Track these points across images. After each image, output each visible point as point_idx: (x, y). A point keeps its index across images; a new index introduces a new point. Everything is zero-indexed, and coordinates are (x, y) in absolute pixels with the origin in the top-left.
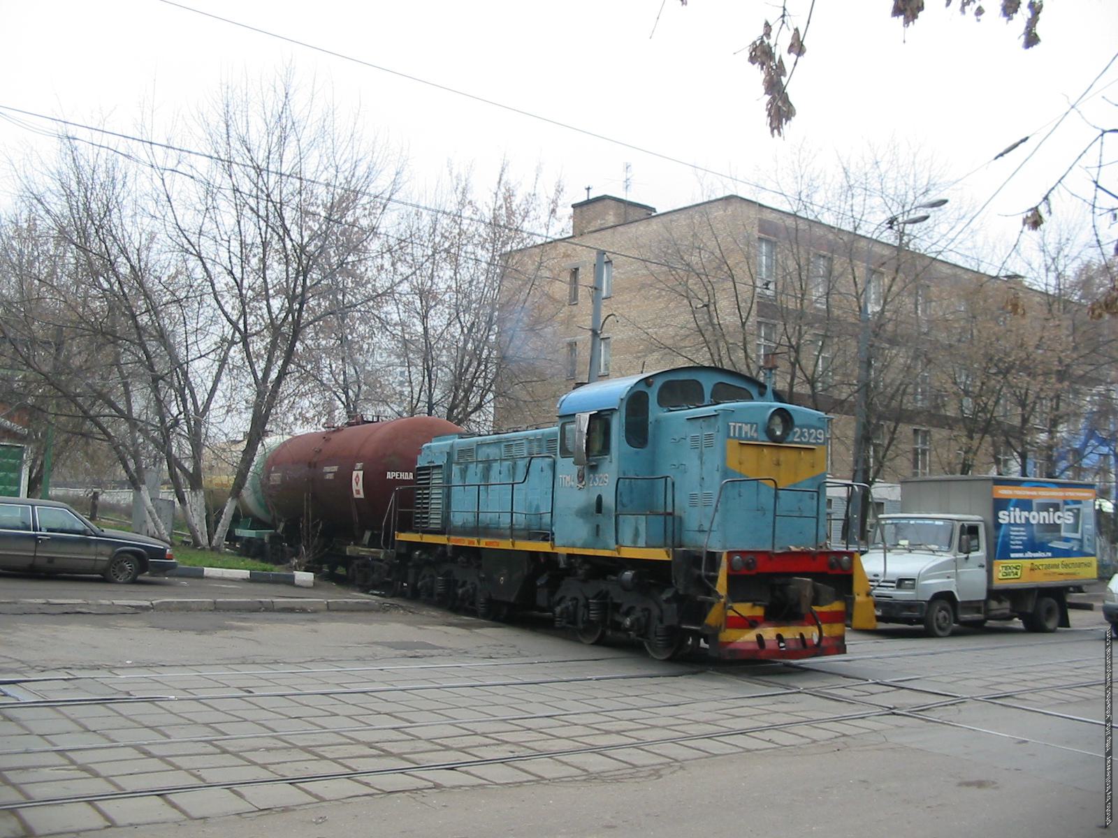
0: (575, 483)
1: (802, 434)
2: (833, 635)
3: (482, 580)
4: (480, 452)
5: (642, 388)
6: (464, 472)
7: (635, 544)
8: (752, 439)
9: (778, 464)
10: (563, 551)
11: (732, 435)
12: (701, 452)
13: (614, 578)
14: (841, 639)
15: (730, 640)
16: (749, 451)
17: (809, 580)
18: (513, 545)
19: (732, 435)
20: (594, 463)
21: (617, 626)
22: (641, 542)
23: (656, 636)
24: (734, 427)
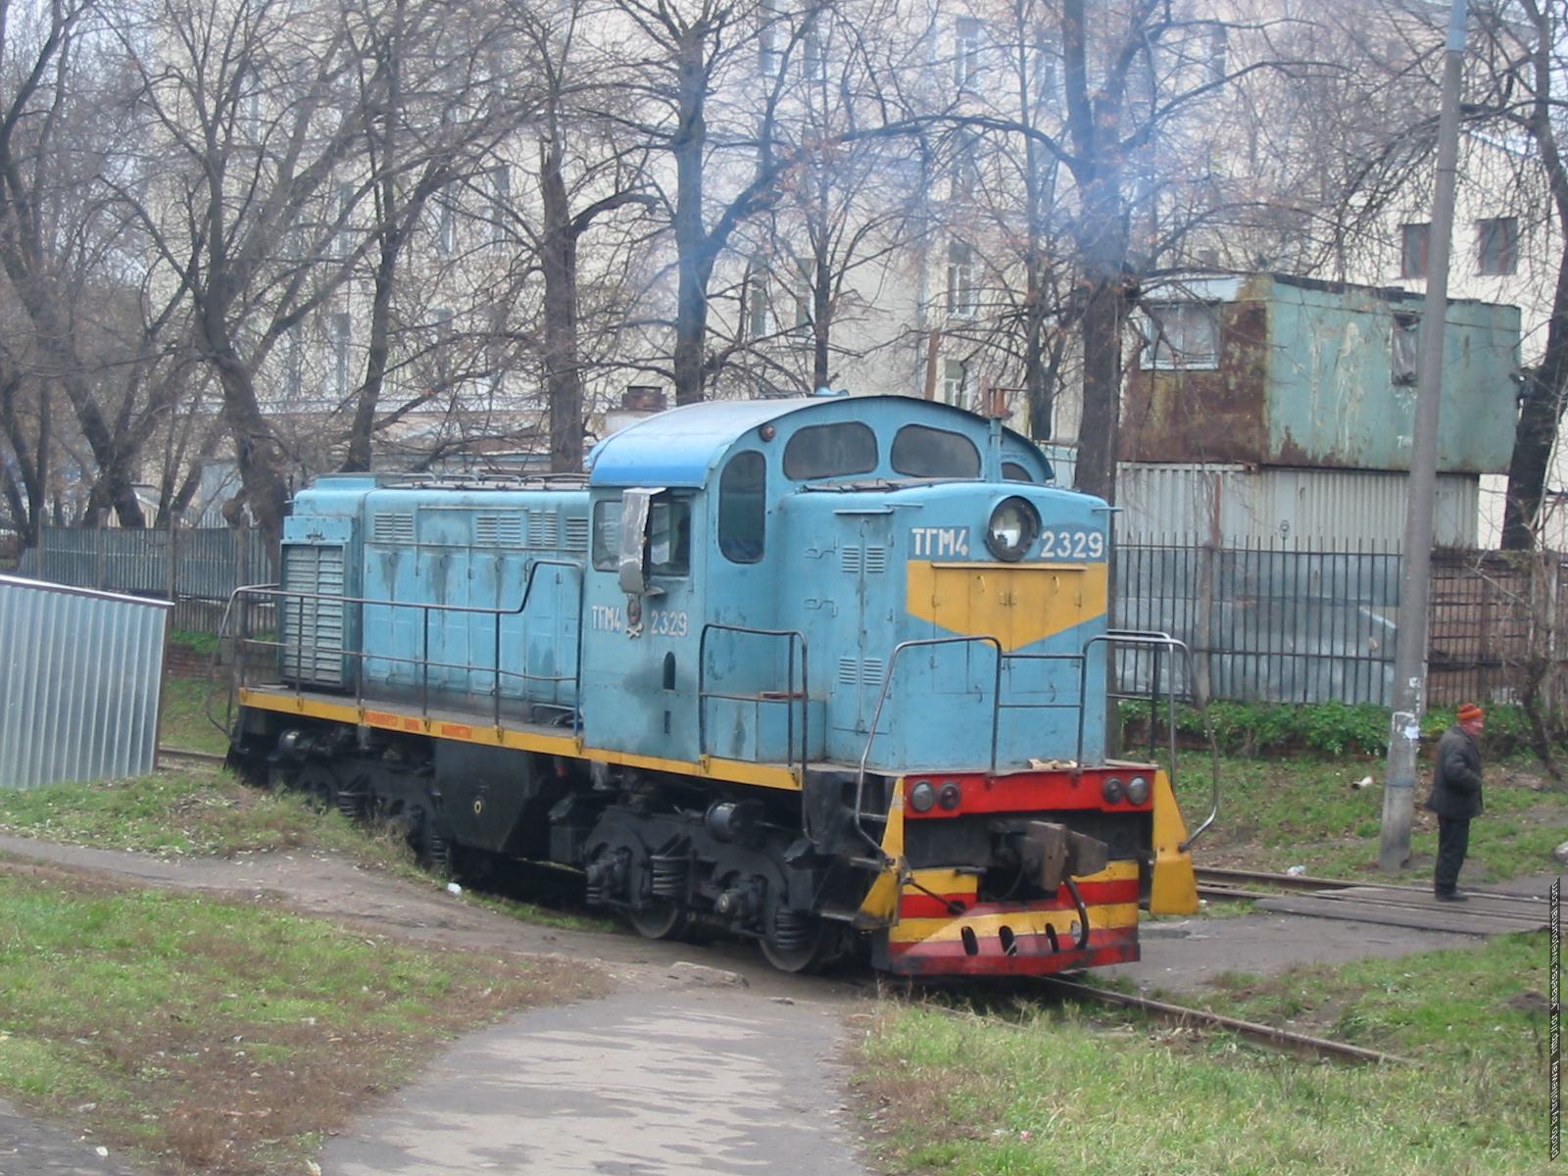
0: (622, 625)
1: (1059, 543)
2: (1114, 925)
3: (434, 800)
4: (425, 525)
5: (754, 445)
6: (391, 564)
7: (736, 755)
8: (957, 557)
9: (1009, 602)
10: (600, 757)
11: (918, 552)
12: (862, 580)
13: (697, 815)
14: (1131, 932)
15: (909, 940)
16: (944, 577)
17: (1057, 827)
18: (500, 736)
19: (918, 552)
20: (661, 591)
21: (707, 905)
22: (748, 751)
23: (778, 929)
24: (923, 536)
